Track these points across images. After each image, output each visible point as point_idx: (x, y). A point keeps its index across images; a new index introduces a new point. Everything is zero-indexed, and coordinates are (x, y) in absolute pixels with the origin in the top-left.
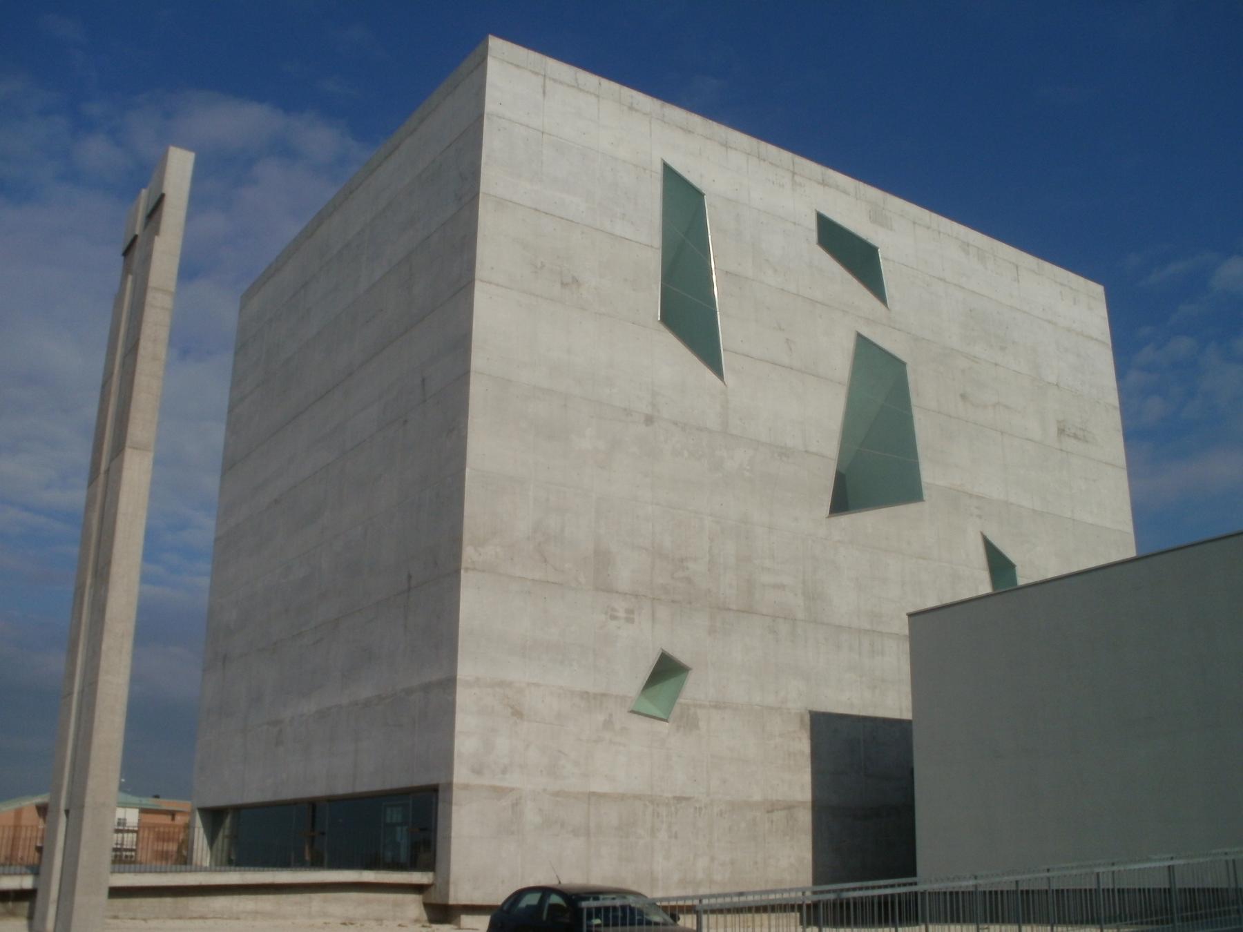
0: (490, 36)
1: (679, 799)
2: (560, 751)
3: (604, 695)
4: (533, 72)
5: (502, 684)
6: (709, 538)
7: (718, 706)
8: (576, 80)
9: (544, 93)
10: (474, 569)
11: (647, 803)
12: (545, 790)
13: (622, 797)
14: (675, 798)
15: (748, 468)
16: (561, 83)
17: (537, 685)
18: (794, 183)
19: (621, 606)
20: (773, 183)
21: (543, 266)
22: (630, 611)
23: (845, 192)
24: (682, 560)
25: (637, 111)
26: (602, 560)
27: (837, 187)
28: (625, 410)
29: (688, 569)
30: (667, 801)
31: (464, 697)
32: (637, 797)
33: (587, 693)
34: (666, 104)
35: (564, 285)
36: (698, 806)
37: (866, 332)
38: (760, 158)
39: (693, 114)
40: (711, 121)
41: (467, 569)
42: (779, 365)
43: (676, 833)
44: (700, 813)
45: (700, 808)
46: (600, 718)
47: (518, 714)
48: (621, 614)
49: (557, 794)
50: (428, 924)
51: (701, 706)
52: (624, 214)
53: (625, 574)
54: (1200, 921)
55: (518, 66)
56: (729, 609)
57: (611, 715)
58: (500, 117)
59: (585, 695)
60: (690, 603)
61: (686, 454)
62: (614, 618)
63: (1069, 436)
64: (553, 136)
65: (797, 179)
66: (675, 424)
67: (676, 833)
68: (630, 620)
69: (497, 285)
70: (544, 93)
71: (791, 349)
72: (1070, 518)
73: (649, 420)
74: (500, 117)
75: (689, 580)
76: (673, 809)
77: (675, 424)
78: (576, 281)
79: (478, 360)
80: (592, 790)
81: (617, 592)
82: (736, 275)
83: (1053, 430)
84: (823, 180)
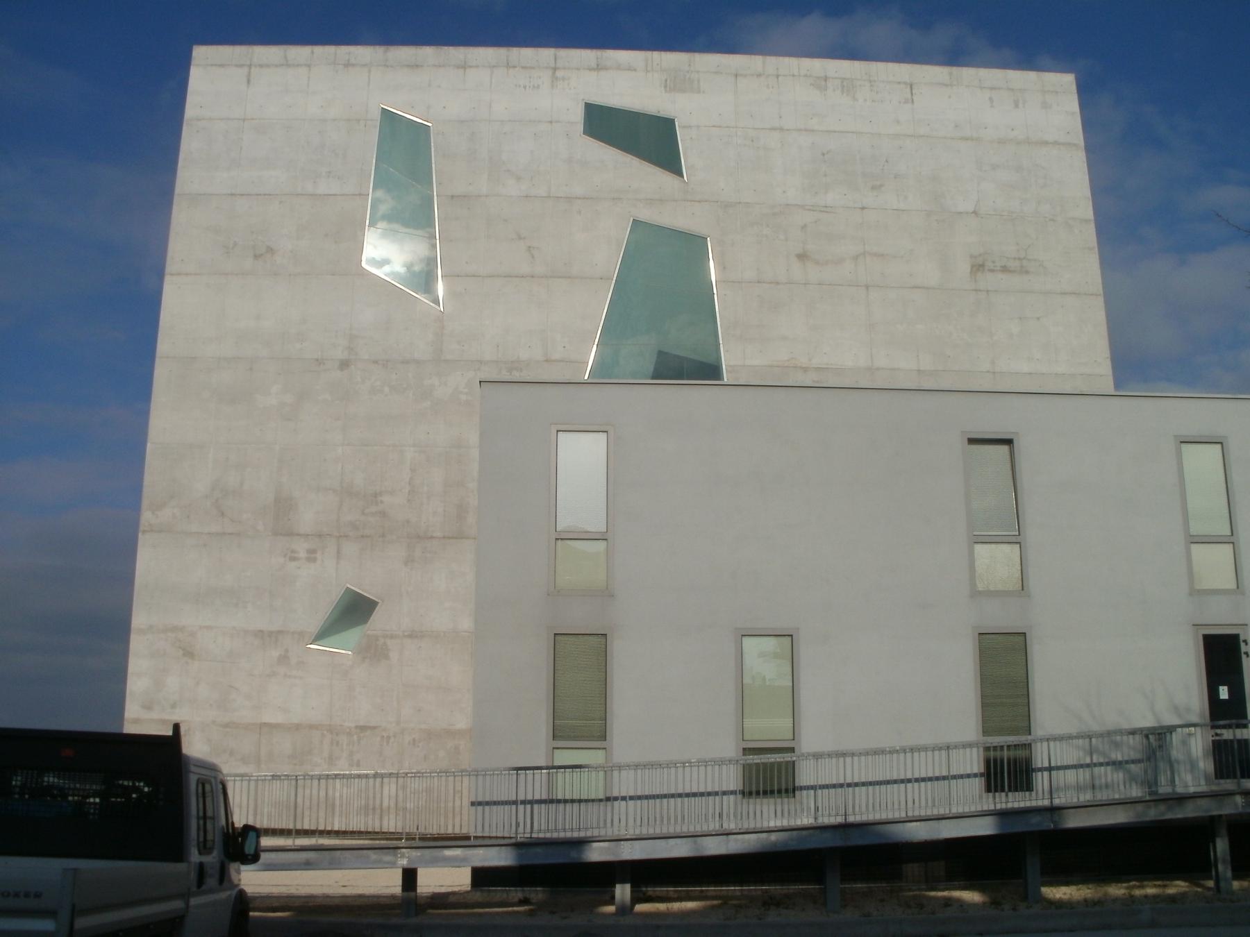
0: (201, 53)
1: (363, 728)
2: (231, 687)
3: (280, 632)
4: (237, 66)
5: (175, 629)
6: (411, 469)
7: (413, 635)
8: (286, 57)
9: (249, 81)
10: (152, 531)
11: (325, 732)
12: (214, 722)
13: (297, 727)
14: (357, 727)
15: (466, 390)
16: (268, 66)
17: (209, 628)
18: (554, 78)
19: (301, 547)
20: (525, 87)
21: (235, 244)
22: (312, 551)
23: (631, 69)
24: (375, 495)
25: (353, 65)
26: (283, 507)
27: (619, 67)
28: (317, 360)
29: (382, 502)
30: (348, 730)
31: (137, 644)
32: (311, 727)
33: (261, 631)
34: (389, 47)
35: (256, 257)
36: (385, 734)
37: (645, 215)
38: (509, 66)
39: (424, 47)
40: (446, 48)
41: (144, 532)
42: (517, 277)
43: (359, 761)
44: (388, 742)
45: (389, 737)
46: (275, 654)
47: (189, 654)
48: (303, 554)
49: (226, 725)
50: (1034, 793)
51: (392, 637)
52: (330, 172)
53: (306, 518)
54: (1103, 781)
55: (222, 66)
56: (432, 537)
57: (287, 651)
58: (198, 120)
59: (260, 634)
60: (383, 536)
61: (386, 389)
62: (293, 559)
63: (992, 271)
64: (256, 119)
65: (559, 74)
66: (376, 362)
67: (359, 761)
68: (311, 560)
69: (187, 274)
70: (249, 81)
71: (533, 257)
72: (988, 372)
73: (344, 365)
74: (198, 120)
75: (383, 514)
76: (355, 737)
77: (376, 362)
78: (270, 250)
79: (164, 346)
80: (263, 721)
81: (298, 535)
82: (465, 196)
83: (964, 267)
84: (598, 65)
